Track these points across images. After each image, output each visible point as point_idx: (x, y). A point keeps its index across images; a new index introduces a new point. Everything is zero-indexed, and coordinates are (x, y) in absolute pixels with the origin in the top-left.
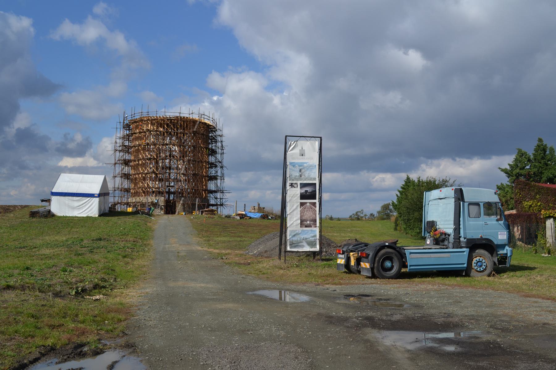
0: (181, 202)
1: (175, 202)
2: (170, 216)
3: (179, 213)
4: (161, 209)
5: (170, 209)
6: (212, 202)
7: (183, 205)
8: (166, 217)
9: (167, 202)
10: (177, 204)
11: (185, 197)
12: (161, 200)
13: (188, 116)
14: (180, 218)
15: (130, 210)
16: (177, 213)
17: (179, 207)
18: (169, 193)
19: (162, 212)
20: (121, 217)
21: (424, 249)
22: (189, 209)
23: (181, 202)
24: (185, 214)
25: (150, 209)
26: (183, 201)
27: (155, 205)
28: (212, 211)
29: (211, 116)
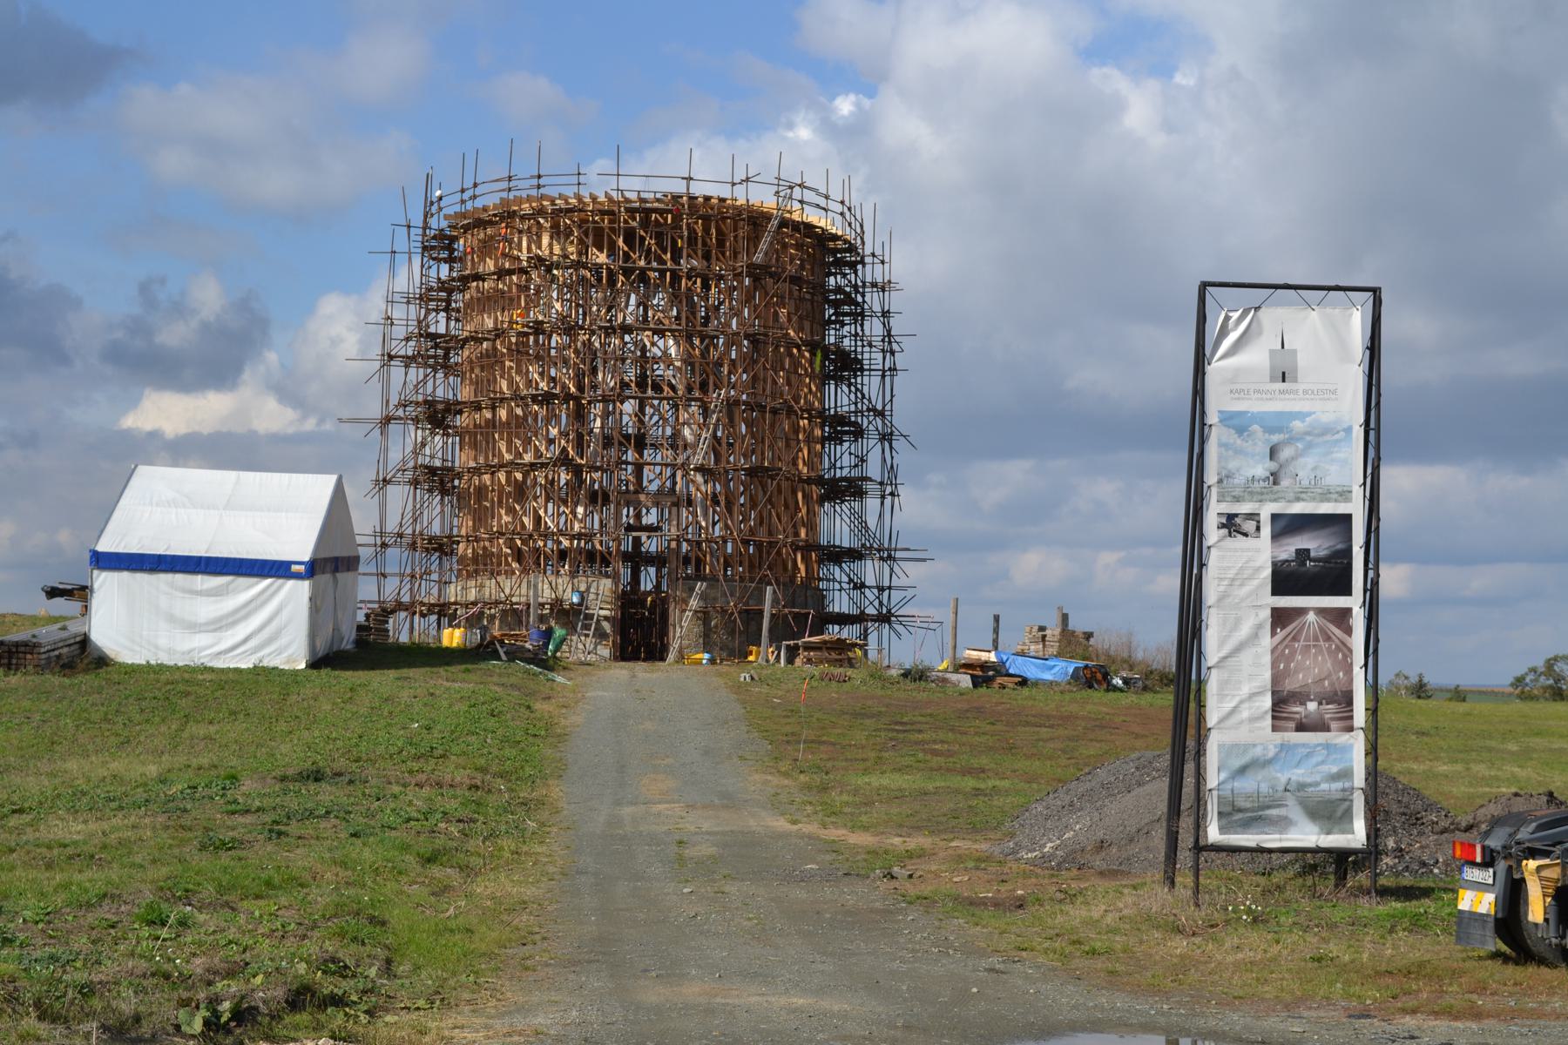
0: (694, 603)
1: (665, 601)
2: (640, 668)
3: (681, 657)
4: (601, 635)
5: (639, 635)
6: (840, 603)
7: (703, 616)
8: (622, 671)
9: (629, 600)
10: (674, 612)
11: (712, 580)
12: (600, 594)
14: (687, 679)
15: (453, 637)
16: (671, 657)
17: (683, 626)
18: (636, 559)
19: (605, 651)
22: (732, 637)
23: (694, 603)
24: (712, 661)
27: (571, 616)
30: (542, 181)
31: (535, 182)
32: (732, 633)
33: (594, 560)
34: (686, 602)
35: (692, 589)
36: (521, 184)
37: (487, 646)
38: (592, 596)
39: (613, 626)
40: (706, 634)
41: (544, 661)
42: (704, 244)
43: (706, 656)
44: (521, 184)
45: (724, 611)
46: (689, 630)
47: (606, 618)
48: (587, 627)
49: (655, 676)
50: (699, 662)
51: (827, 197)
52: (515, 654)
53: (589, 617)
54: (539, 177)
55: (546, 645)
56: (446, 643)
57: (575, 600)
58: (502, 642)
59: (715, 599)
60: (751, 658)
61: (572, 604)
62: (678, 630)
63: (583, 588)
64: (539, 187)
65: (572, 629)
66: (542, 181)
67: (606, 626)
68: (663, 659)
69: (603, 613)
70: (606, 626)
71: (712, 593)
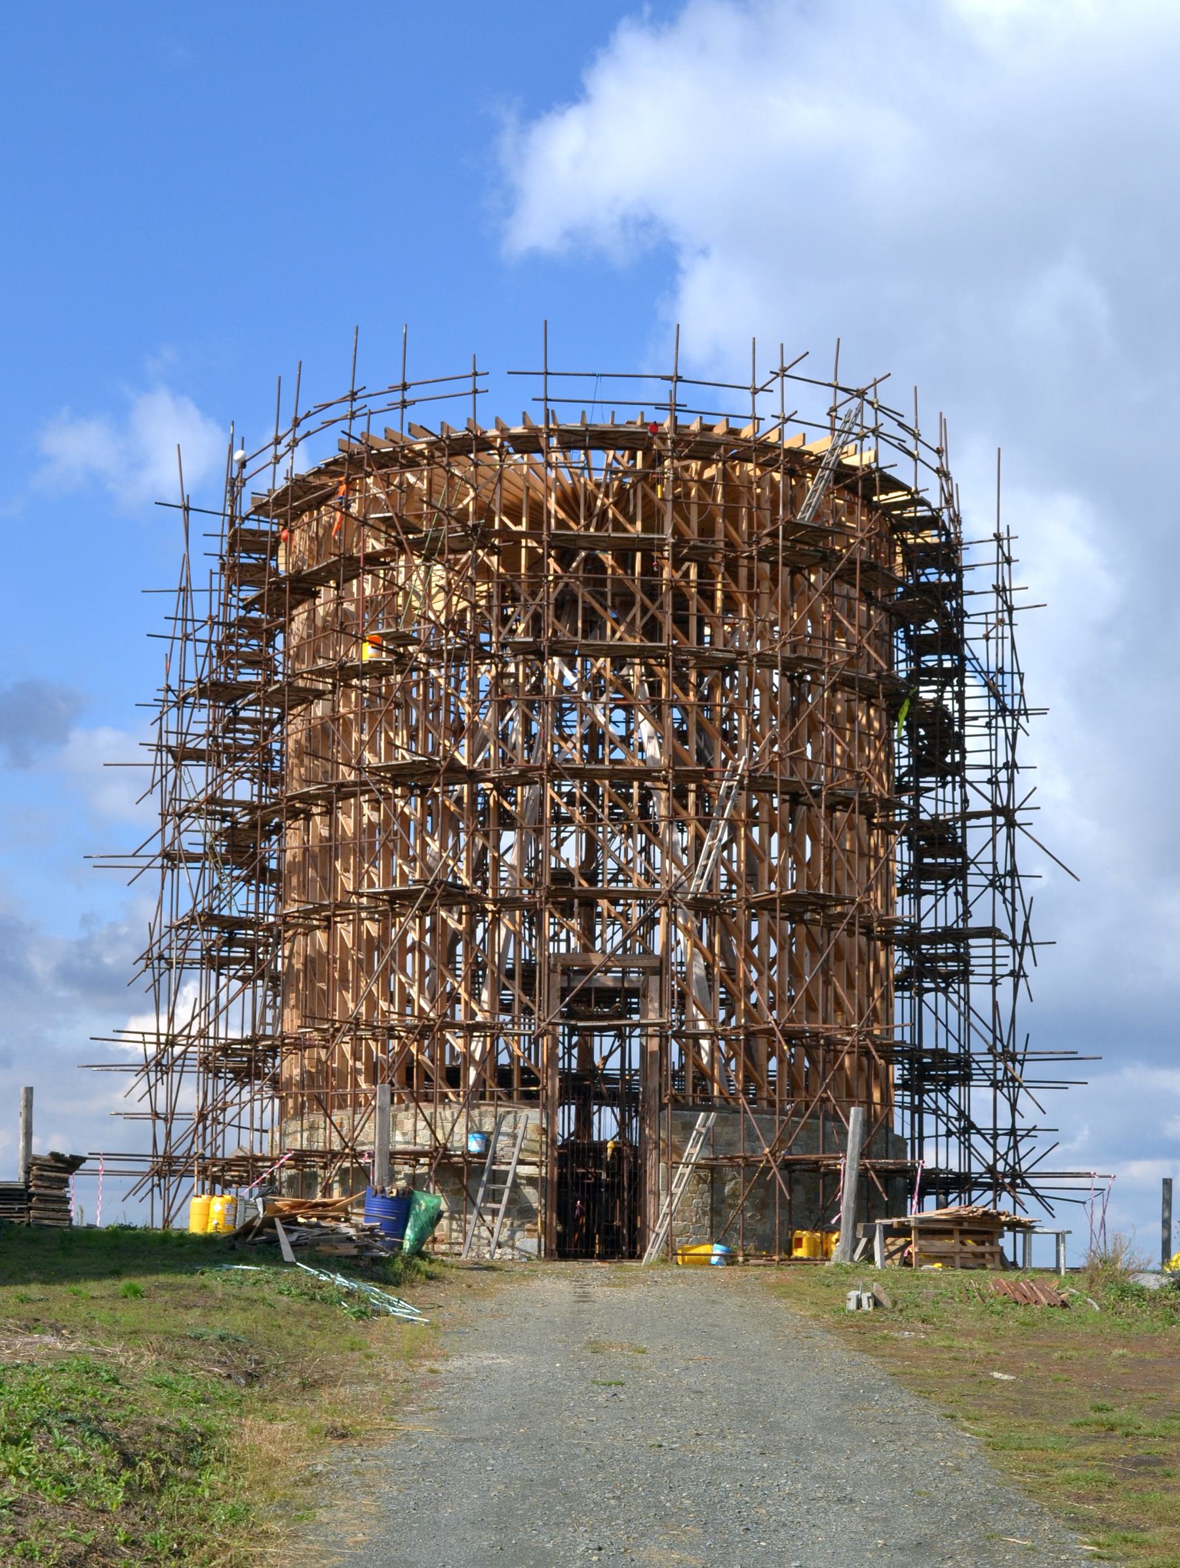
0: (693, 1151)
1: (638, 1153)
2: (596, 1275)
3: (670, 1252)
4: (520, 1211)
5: (593, 1213)
6: (939, 1155)
7: (711, 1174)
8: (560, 1286)
9: (575, 1155)
10: (655, 1170)
11: (727, 1107)
12: (521, 1138)
13: (741, 402)
14: (684, 1297)
15: (206, 1213)
16: (652, 1251)
17: (672, 1196)
18: (584, 1088)
19: (529, 1243)
20: (142, 1282)
21: (53, 1210)
22: (776, 1208)
23: (693, 1151)
24: (729, 1259)
25: (402, 1206)
26: (710, 1141)
27: (460, 1175)
28: (987, 1228)
29: (931, 436)
30: (409, 395)
31: (397, 397)
32: (763, 1206)
33: (512, 1084)
34: (679, 1151)
35: (688, 1127)
36: (374, 404)
37: (260, 1232)
38: (503, 1141)
39: (544, 1194)
40: (716, 1209)
41: (372, 1262)
42: (702, 508)
43: (718, 1249)
44: (374, 404)
45: (750, 1165)
46: (684, 1201)
47: (531, 1181)
48: (495, 1196)
49: (634, 1294)
50: (703, 1262)
51: (916, 436)
52: (317, 1251)
53: (498, 1177)
54: (405, 387)
55: (398, 1228)
56: (195, 1227)
57: (474, 1146)
58: (290, 1222)
59: (730, 1144)
60: (799, 1253)
61: (466, 1154)
62: (665, 1201)
63: (488, 1126)
64: (404, 404)
65: (463, 1199)
66: (409, 395)
67: (532, 1195)
68: (635, 1256)
69: (524, 1170)
70: (532, 1195)
71: (726, 1133)
